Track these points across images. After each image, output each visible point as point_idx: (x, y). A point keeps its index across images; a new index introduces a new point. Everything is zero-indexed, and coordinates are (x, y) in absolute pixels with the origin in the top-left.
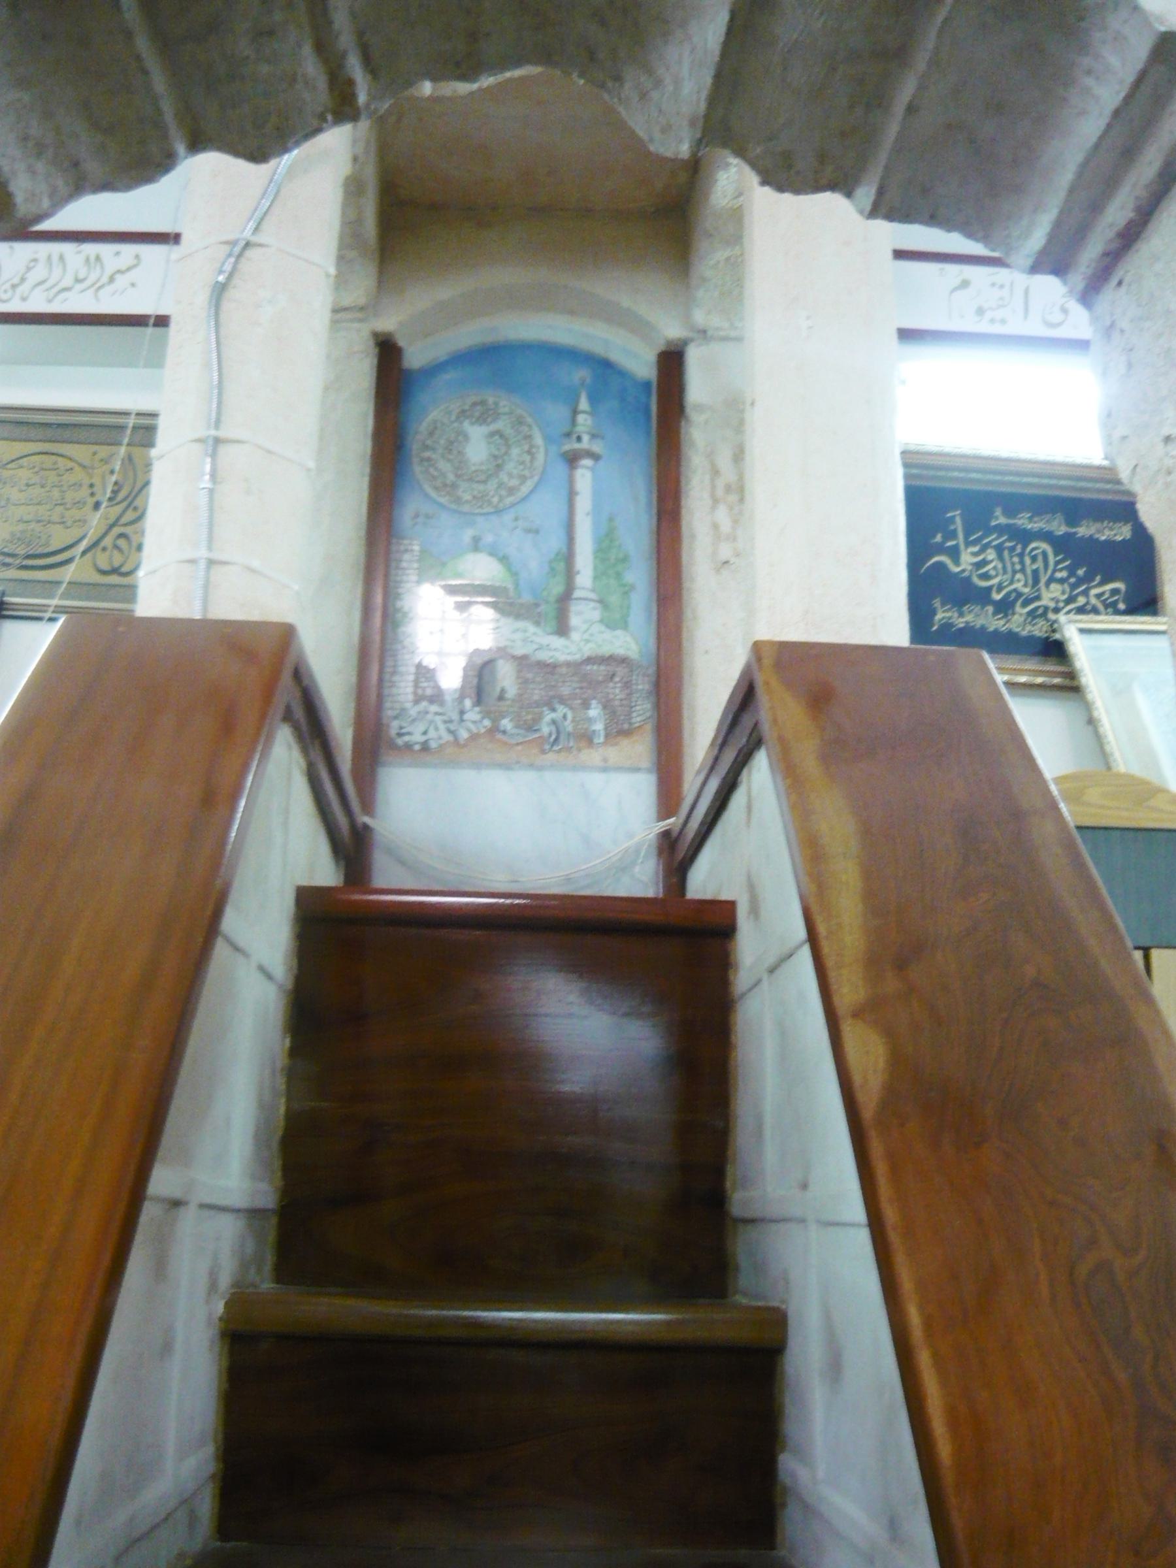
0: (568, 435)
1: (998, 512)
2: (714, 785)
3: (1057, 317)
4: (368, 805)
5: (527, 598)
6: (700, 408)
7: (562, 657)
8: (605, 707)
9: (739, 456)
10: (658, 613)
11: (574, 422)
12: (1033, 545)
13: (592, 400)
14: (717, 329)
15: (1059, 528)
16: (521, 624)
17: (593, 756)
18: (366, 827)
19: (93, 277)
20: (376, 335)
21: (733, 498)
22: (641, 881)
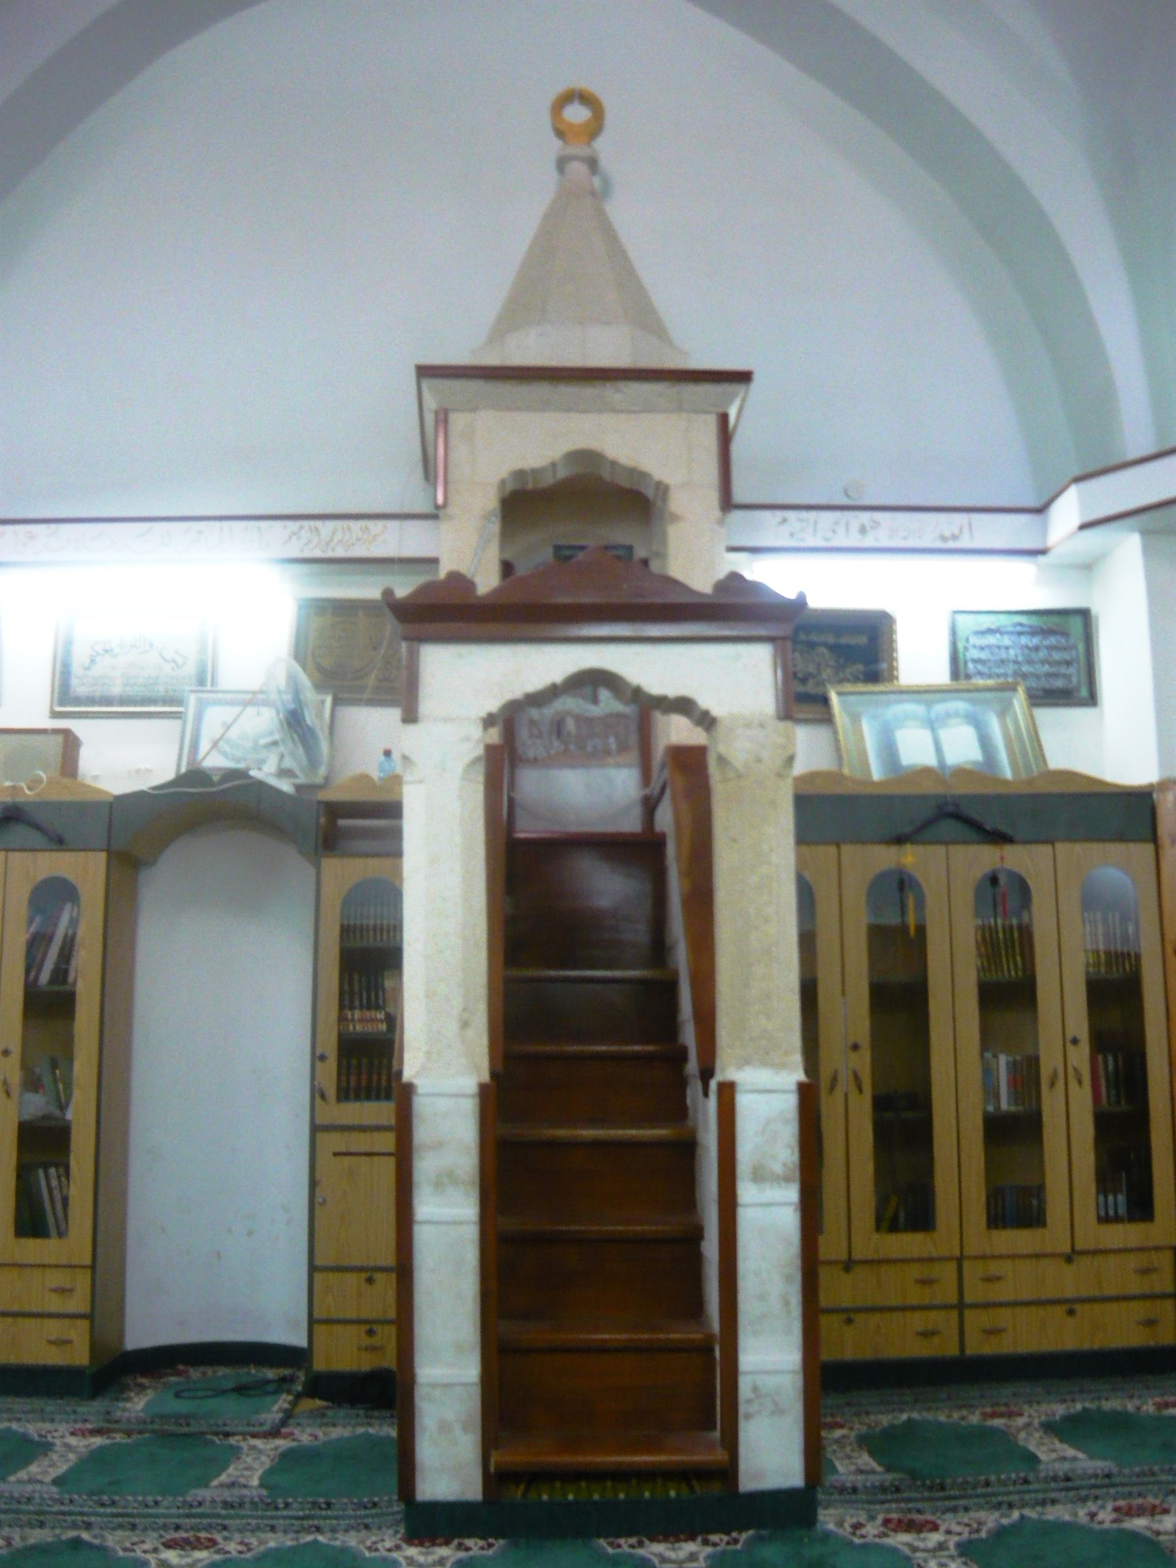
15: (831, 640)
17: (611, 760)
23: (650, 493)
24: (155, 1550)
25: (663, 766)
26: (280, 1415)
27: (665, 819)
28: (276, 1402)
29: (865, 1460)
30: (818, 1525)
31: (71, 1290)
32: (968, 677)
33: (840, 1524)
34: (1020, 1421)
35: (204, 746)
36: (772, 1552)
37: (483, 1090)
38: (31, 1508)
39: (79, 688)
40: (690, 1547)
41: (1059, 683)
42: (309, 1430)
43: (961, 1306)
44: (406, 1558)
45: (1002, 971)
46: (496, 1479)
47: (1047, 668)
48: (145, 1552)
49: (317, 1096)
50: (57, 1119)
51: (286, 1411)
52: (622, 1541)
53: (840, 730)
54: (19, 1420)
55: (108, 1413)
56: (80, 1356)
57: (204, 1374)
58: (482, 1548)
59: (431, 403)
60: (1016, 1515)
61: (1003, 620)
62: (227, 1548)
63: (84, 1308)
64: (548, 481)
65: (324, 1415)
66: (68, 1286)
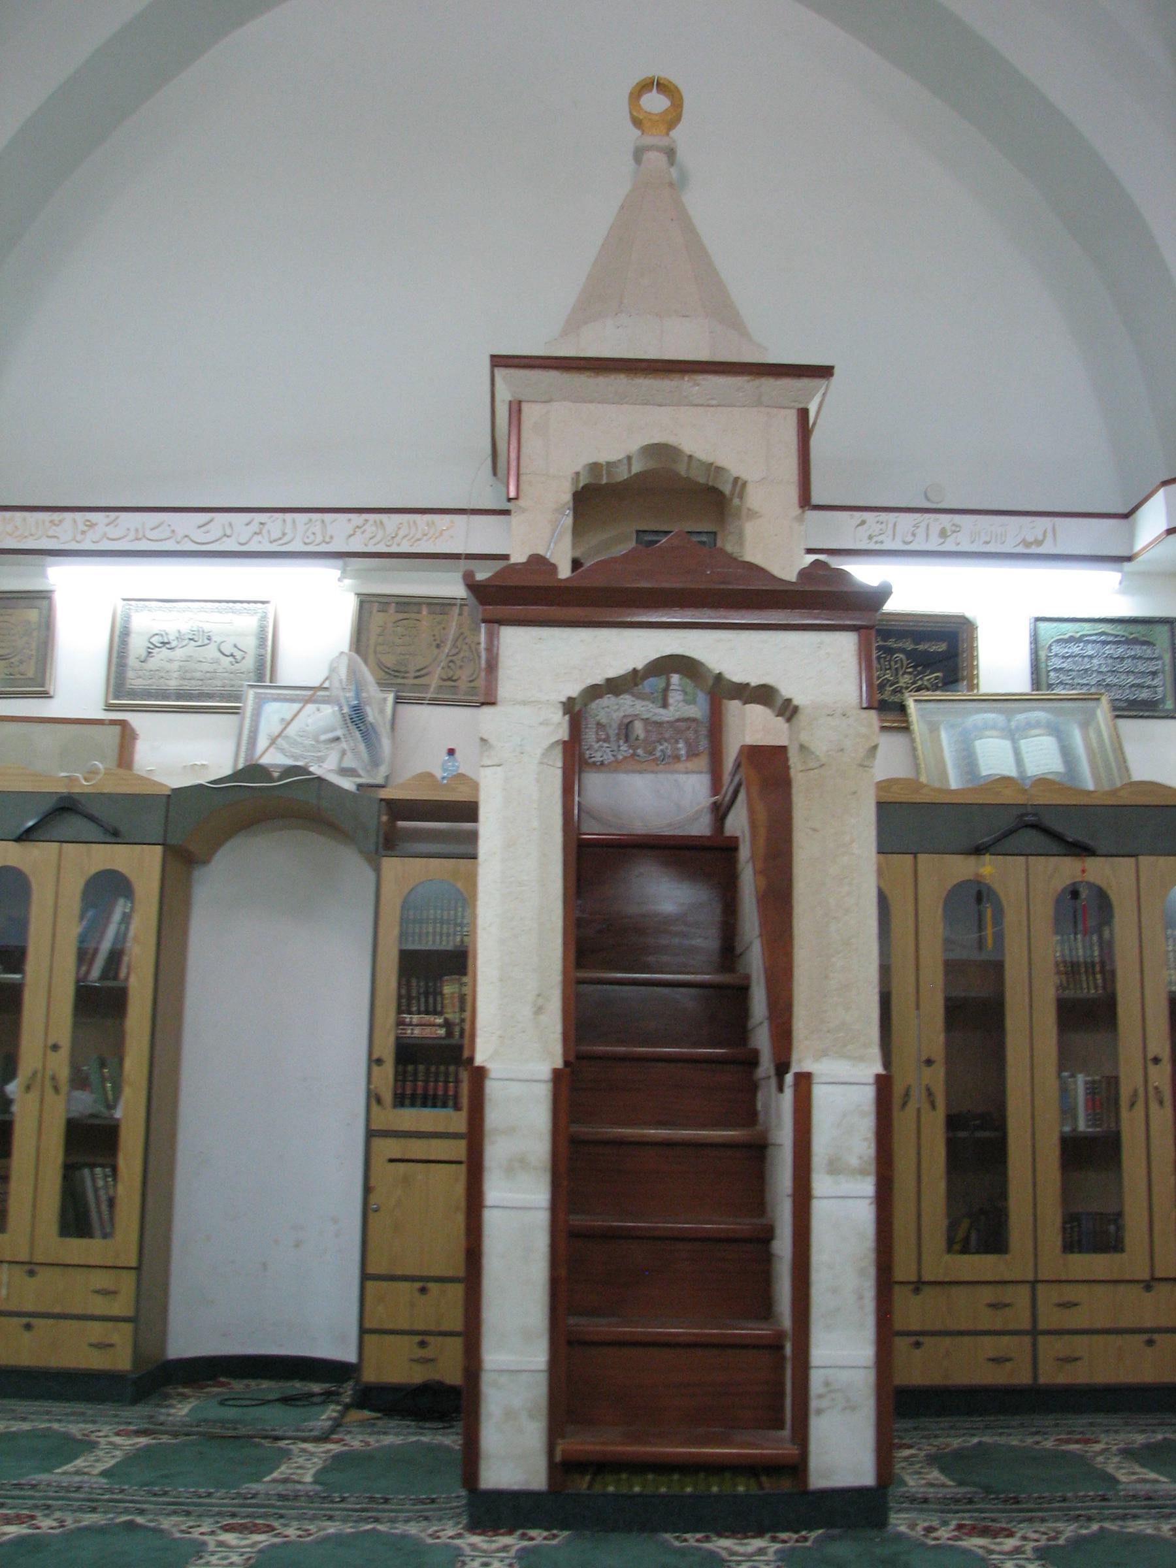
15: (909, 646)
17: (680, 766)
23: (727, 489)
24: (212, 1533)
25: (738, 766)
26: (329, 1423)
27: (738, 823)
28: (323, 1412)
29: (935, 1475)
30: (889, 1527)
31: (115, 1293)
32: (1050, 686)
33: (912, 1526)
34: (1098, 1447)
35: (262, 742)
36: (843, 1549)
37: (557, 1075)
38: (82, 1496)
39: (135, 681)
40: (757, 1543)
41: (1144, 695)
42: (360, 1437)
43: (1034, 1332)
44: (470, 1545)
45: (1082, 988)
46: (562, 1468)
47: (1131, 679)
48: (202, 1534)
49: (373, 1102)
50: (105, 1118)
51: (335, 1419)
52: (688, 1536)
53: (918, 740)
54: (60, 1421)
55: (152, 1417)
56: (122, 1361)
57: (247, 1386)
58: (545, 1538)
59: (504, 395)
60: (1095, 1527)
61: (1087, 628)
62: (286, 1533)
63: (129, 1312)
64: (622, 475)
65: (374, 1425)
66: (112, 1288)
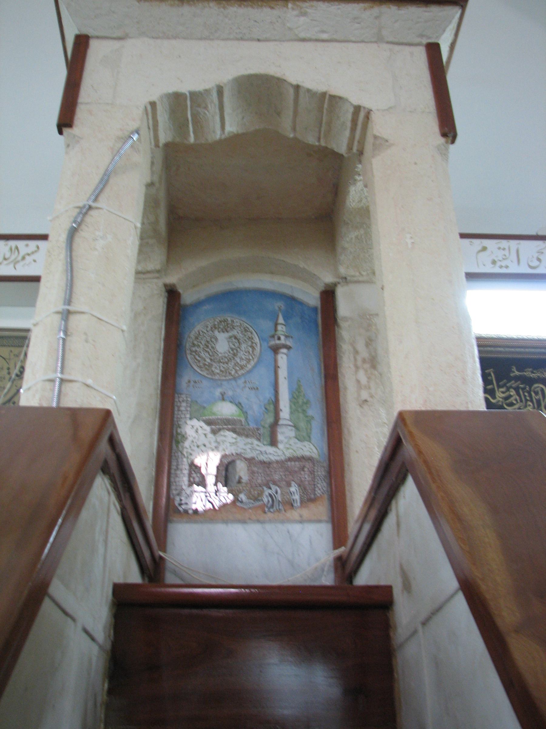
0: (273, 336)
1: (514, 369)
2: (367, 528)
3: (535, 263)
4: (163, 546)
5: (252, 425)
6: (345, 319)
7: (273, 458)
8: (299, 486)
9: (369, 342)
10: (328, 431)
11: (276, 330)
12: (536, 385)
13: (286, 318)
14: (353, 276)
16: (249, 440)
17: (294, 514)
18: (161, 558)
19: (13, 257)
20: (165, 285)
21: (367, 366)
22: (328, 579)
